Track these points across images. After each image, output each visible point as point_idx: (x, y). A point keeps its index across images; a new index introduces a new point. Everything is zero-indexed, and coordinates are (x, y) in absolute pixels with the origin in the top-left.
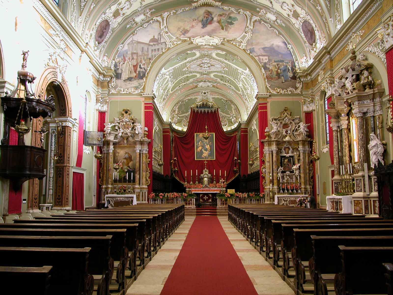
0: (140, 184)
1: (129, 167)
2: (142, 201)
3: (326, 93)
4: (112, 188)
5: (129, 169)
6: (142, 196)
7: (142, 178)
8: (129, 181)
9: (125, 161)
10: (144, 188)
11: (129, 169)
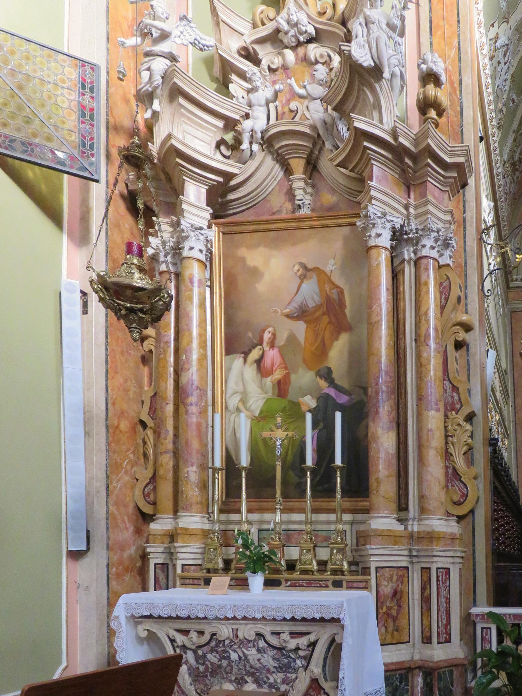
0: (402, 506)
1: (327, 375)
2: (427, 640)
3: (120, 23)
4: (205, 534)
5: (332, 392)
6: (426, 600)
7: (421, 460)
8: (294, 491)
9: (300, 328)
10: (431, 537)
11: (332, 392)
